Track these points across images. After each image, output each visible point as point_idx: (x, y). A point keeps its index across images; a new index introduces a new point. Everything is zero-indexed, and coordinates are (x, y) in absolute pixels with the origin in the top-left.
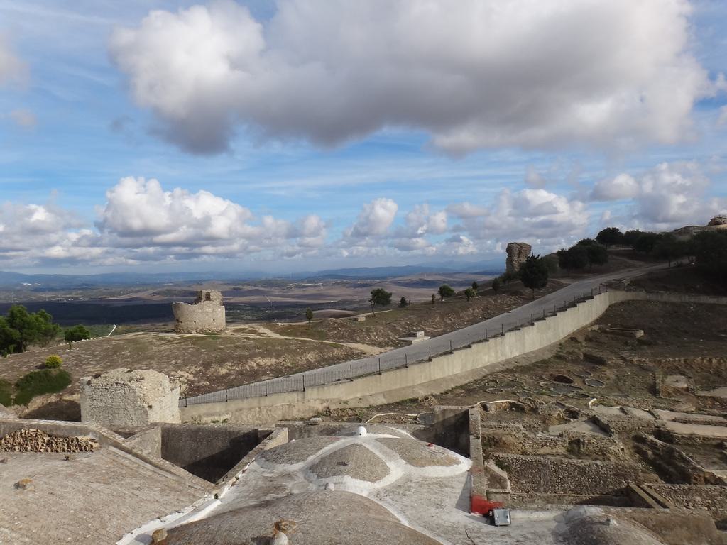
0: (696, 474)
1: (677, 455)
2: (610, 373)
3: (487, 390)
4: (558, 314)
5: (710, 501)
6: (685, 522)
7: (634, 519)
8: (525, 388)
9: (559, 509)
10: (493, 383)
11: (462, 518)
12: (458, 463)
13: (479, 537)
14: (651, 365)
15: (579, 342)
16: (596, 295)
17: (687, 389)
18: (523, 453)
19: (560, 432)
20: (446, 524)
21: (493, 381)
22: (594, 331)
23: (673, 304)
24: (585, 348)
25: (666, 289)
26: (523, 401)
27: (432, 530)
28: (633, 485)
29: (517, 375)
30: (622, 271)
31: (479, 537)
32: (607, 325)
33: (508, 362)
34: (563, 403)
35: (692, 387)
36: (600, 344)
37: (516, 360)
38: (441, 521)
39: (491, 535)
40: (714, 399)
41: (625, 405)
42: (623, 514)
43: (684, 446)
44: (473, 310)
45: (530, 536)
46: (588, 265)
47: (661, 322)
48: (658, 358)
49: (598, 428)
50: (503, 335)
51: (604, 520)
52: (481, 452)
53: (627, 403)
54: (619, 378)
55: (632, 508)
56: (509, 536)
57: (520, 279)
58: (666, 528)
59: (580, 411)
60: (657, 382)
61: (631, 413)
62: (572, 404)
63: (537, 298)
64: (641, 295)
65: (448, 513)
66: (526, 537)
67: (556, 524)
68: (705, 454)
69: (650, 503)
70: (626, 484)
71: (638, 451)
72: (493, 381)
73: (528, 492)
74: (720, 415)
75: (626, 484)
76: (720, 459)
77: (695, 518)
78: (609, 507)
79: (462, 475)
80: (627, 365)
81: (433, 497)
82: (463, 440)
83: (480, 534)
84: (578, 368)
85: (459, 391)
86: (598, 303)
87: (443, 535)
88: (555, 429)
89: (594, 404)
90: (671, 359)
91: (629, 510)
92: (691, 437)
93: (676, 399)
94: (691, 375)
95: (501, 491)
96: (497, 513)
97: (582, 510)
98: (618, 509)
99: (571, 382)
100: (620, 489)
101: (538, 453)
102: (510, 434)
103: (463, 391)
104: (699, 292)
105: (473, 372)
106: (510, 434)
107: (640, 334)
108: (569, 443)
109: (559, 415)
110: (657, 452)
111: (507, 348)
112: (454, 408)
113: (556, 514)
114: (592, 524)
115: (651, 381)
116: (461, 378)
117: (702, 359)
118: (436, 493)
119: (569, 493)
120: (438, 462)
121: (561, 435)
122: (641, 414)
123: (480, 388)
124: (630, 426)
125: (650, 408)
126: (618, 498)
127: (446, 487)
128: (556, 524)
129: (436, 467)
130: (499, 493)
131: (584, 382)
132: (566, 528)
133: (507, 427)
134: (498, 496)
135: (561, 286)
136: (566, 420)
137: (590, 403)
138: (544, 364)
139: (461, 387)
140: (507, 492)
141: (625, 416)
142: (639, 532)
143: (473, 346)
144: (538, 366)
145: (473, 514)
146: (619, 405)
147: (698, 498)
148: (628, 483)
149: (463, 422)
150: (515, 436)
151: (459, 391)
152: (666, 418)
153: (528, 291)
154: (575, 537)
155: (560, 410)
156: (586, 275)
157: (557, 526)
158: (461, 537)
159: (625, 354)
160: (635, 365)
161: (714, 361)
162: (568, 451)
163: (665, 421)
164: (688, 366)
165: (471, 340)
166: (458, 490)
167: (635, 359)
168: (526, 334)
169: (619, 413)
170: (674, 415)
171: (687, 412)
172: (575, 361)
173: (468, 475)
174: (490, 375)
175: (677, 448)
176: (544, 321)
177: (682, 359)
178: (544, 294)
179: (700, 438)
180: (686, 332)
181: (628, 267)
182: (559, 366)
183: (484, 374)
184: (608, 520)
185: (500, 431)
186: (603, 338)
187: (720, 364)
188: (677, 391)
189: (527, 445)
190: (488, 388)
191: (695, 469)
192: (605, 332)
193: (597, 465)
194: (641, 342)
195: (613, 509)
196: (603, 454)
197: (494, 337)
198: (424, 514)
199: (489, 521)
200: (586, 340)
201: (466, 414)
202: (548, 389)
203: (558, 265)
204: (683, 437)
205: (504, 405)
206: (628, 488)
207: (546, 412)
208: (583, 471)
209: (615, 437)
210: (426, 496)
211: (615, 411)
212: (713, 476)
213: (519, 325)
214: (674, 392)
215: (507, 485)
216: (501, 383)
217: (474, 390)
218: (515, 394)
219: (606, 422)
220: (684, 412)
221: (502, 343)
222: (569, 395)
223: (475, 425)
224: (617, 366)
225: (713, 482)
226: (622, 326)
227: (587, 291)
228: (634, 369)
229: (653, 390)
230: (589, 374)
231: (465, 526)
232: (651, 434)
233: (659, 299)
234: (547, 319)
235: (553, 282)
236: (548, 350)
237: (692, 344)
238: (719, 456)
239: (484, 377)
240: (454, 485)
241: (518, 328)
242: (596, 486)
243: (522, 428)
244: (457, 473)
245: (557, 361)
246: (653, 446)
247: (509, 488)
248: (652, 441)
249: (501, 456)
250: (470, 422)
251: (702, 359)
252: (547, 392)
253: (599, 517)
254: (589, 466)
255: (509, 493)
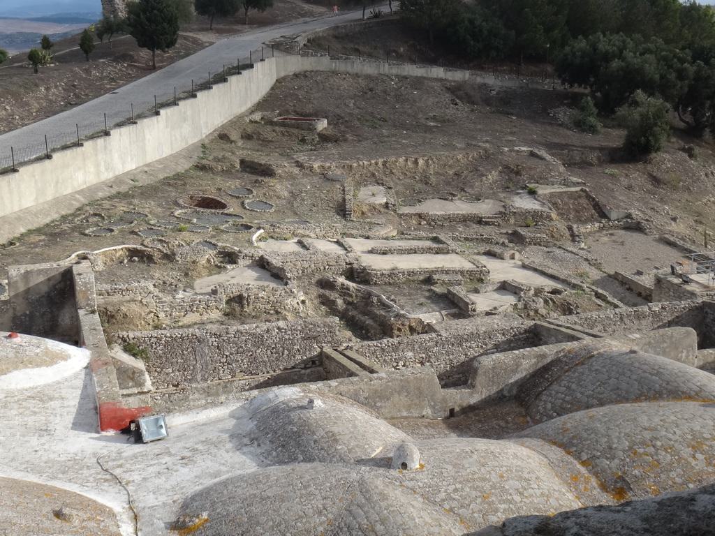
0: (400, 322)
1: (375, 300)
2: (281, 188)
3: (87, 232)
4: (199, 94)
5: (424, 355)
6: (404, 388)
7: (341, 394)
8: (152, 222)
9: (238, 399)
10: (95, 219)
11: (88, 444)
12: (65, 357)
13: (121, 466)
14: (339, 172)
15: (232, 142)
16: (257, 62)
17: (386, 206)
18: (156, 327)
19: (213, 287)
20: (63, 458)
21: (95, 215)
22: (256, 122)
23: (368, 77)
24: (242, 151)
25: (358, 52)
26: (150, 244)
27: (41, 473)
28: (328, 350)
29: (136, 201)
30: (294, 21)
31: (121, 466)
32: (273, 111)
33: (118, 180)
34: (213, 241)
35: (392, 201)
36: (265, 143)
37: (132, 176)
38: (52, 456)
39: (139, 458)
40: (420, 216)
41: (303, 236)
42: (326, 390)
43: (384, 287)
44: (47, 89)
45: (200, 447)
46: (243, 10)
47: (351, 105)
48: (348, 162)
49: (268, 275)
50: (107, 134)
51: (305, 402)
52: (102, 336)
53: (307, 233)
54: (294, 195)
55: (339, 380)
56: (170, 454)
57: (131, 33)
58: (381, 398)
59: (240, 252)
60: (347, 197)
61: (314, 247)
62: (227, 242)
63: (161, 68)
64: (322, 63)
65: (61, 440)
66: (194, 450)
67: (234, 422)
68: (410, 294)
69: (354, 370)
70: (319, 350)
71: (325, 301)
72: (95, 215)
73: (177, 386)
74: (427, 239)
75: (319, 350)
76: (429, 298)
77: (416, 378)
78: (308, 384)
79: (76, 376)
80: (305, 175)
81: (30, 421)
82: (65, 319)
83: (121, 461)
84: (232, 184)
85: (35, 238)
86: (261, 77)
87: (60, 476)
88: (204, 283)
89: (260, 239)
90: (365, 162)
91: (333, 383)
92: (393, 273)
93: (373, 221)
94: (392, 184)
95: (136, 390)
96: (145, 425)
97: (271, 395)
98: (320, 384)
99: (223, 206)
100: (310, 358)
101: (180, 324)
102: (134, 301)
103: (43, 237)
104: (401, 58)
105: (57, 202)
106: (134, 301)
107: (322, 125)
108: (227, 302)
109: (208, 261)
110: (350, 300)
111: (116, 156)
112: (44, 269)
113: (234, 408)
114: (289, 411)
115: (339, 197)
116: (36, 215)
117: (406, 160)
118: (35, 413)
119: (239, 375)
120: (31, 363)
121: (214, 292)
122: (326, 247)
123: (73, 229)
124: (313, 266)
125: (339, 237)
126: (308, 371)
127: (51, 399)
128: (234, 422)
129: (28, 370)
130: (135, 395)
131: (243, 204)
132: (251, 425)
133: (127, 290)
134: (131, 400)
135: (200, 46)
136: (220, 267)
137: (254, 238)
138: (178, 180)
139: (39, 231)
140: (145, 390)
141: (306, 252)
142: (351, 409)
143: (56, 156)
144: (169, 185)
145: (104, 433)
146: (296, 236)
147: (410, 354)
148: (321, 348)
149: (63, 290)
150: (141, 302)
151: (35, 238)
152: (360, 250)
153: (145, 54)
154: (267, 434)
155: (210, 253)
156: (239, 27)
157: (235, 426)
158: (92, 471)
159: (302, 158)
160: (316, 174)
161: (421, 162)
162: (226, 315)
163: (359, 254)
164: (388, 172)
165: (50, 146)
166: (73, 400)
167: (316, 165)
168: (146, 131)
169: (297, 248)
170: (370, 244)
171: (387, 239)
172: (227, 173)
173: (86, 374)
174: (89, 204)
175: (375, 290)
176: (176, 107)
177: (381, 161)
178: (172, 60)
179: (403, 273)
180: (385, 121)
181: (303, 16)
182: (204, 183)
183: (77, 205)
184: (311, 402)
185: (116, 298)
186: (268, 132)
187: (428, 165)
188: (373, 208)
189: (162, 315)
190: (88, 227)
191: (398, 316)
192: (271, 123)
193: (279, 328)
194: (324, 138)
195: (313, 386)
196: (277, 313)
197: (92, 137)
198: (19, 450)
199: (132, 439)
200: (242, 137)
201: (67, 277)
202: (189, 222)
203: (193, 8)
204: (382, 274)
205: (118, 255)
206: (321, 354)
207: (188, 259)
208: (259, 340)
209: (293, 285)
210: (17, 421)
211: (291, 246)
212: (421, 322)
213: (135, 114)
214: (370, 211)
215: (145, 381)
216: (109, 217)
217: (62, 234)
218: (136, 234)
219: (279, 265)
220: (383, 239)
221: (105, 148)
222: (222, 227)
223: (85, 292)
224: (292, 177)
225: (420, 329)
226: (297, 113)
227: (243, 55)
228: (316, 179)
229: (342, 211)
230: (250, 192)
231: (94, 454)
232: (341, 275)
233: (349, 69)
234: (181, 103)
235: (186, 38)
236: (185, 157)
237: (394, 139)
238: (427, 294)
239: (79, 209)
240: (63, 395)
241: (131, 121)
242: (277, 359)
243: (152, 288)
244: (68, 374)
245: (201, 173)
246: (344, 291)
247: (148, 384)
248: (343, 285)
249: (131, 336)
250: (78, 288)
251: (406, 160)
252: (188, 225)
253: (297, 400)
254: (268, 331)
255: (149, 392)
